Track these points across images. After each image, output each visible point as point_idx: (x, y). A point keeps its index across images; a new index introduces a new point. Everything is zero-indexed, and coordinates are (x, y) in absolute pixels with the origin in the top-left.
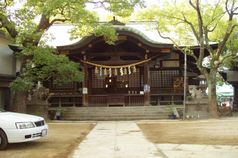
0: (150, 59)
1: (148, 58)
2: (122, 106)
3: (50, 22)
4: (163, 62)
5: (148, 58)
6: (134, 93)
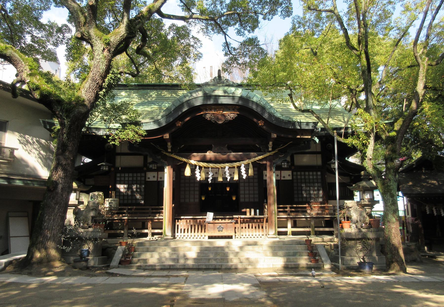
4: (295, 156)
5: (273, 149)
6: (255, 214)
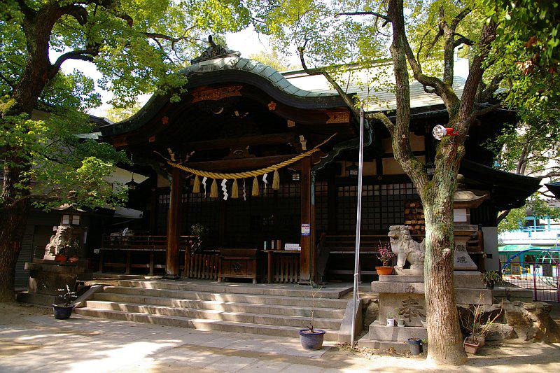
0: (315, 150)
1: (310, 147)
2: (249, 281)
3: (335, 92)
5: (310, 147)
